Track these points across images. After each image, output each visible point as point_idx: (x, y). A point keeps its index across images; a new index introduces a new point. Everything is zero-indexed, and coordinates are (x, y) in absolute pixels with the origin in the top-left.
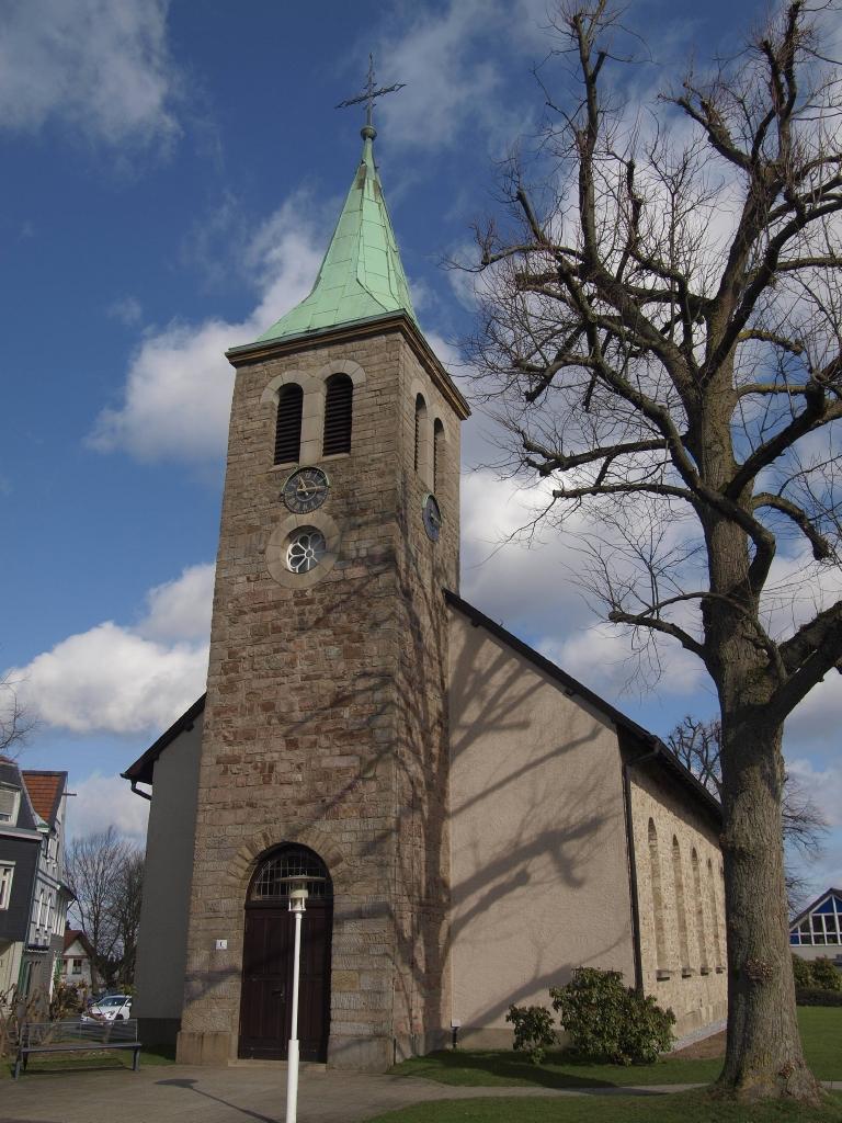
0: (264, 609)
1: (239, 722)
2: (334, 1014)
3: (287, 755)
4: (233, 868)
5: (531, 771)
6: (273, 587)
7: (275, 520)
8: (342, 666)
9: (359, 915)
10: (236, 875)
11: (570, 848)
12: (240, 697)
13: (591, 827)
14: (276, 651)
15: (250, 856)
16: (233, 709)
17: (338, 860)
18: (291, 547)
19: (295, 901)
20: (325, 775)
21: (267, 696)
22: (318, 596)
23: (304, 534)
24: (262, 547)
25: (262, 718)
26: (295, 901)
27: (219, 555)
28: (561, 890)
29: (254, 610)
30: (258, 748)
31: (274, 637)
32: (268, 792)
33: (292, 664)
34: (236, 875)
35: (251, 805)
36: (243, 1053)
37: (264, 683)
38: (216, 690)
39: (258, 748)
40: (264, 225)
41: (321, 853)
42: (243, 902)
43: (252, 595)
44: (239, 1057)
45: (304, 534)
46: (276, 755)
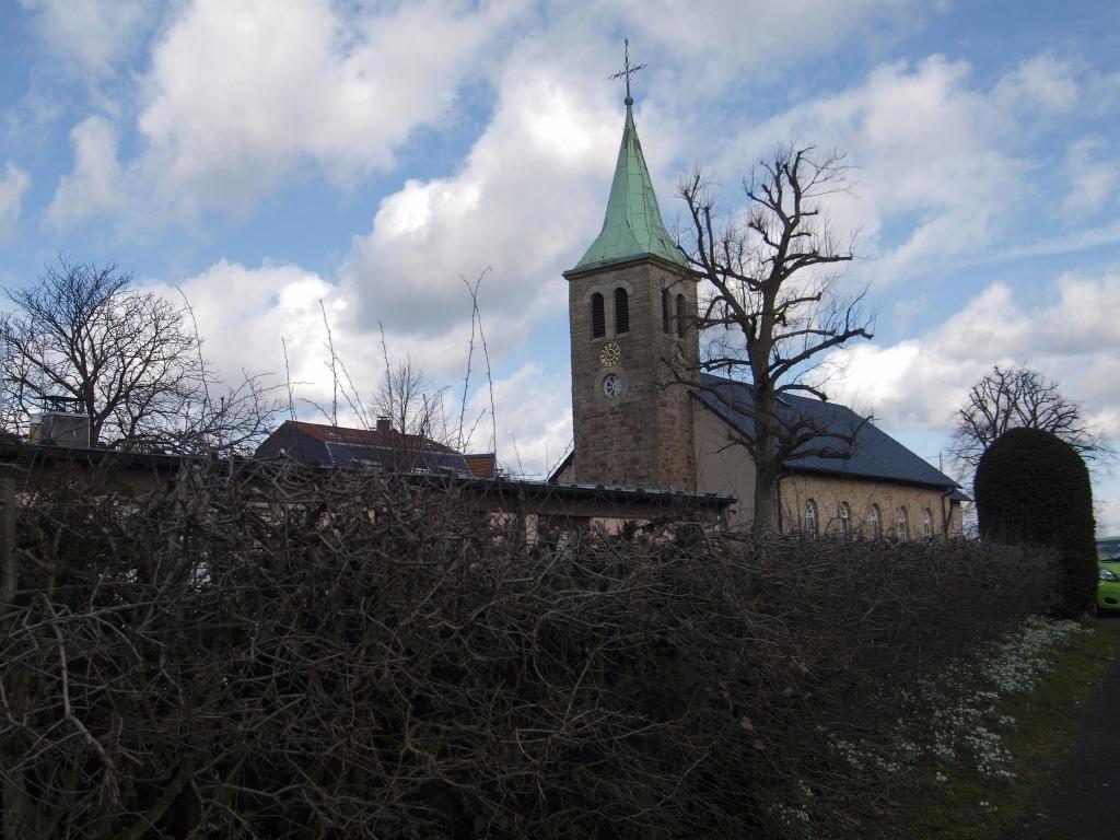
1: (591, 472)
21: (601, 459)
22: (620, 410)
25: (601, 469)
43: (590, 409)
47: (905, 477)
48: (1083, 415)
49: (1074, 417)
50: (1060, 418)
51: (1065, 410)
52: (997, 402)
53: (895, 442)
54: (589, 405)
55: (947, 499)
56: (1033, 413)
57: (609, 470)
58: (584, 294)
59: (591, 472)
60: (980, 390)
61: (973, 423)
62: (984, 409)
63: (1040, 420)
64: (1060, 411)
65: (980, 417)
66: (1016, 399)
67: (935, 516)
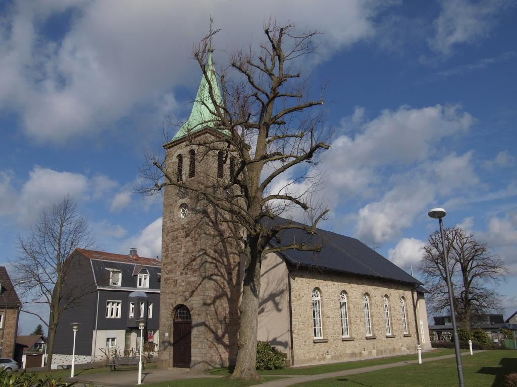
0: (174, 231)
1: (169, 267)
2: (192, 355)
3: (180, 277)
4: (168, 312)
5: (267, 273)
6: (176, 224)
7: (176, 201)
8: (192, 249)
9: (197, 325)
10: (169, 314)
11: (277, 299)
12: (169, 260)
13: (282, 292)
14: (177, 244)
15: (172, 308)
16: (168, 263)
17: (192, 309)
18: (182, 210)
19: (141, 326)
20: (189, 283)
21: (175, 259)
22: (187, 226)
23: (183, 206)
24: (173, 211)
25: (174, 266)
26: (141, 326)
27: (163, 214)
28: (275, 312)
29: (172, 232)
30: (173, 275)
31: (177, 240)
32: (176, 289)
33: (181, 248)
34: (169, 314)
35: (172, 293)
36: (174, 366)
37: (174, 255)
38: (163, 257)
39: (173, 275)
40: (31, 173)
41: (188, 307)
42: (172, 322)
43: (171, 227)
44: (174, 366)
45: (183, 206)
46: (178, 278)
47: (387, 276)
48: (488, 250)
49: (483, 251)
50: (476, 251)
51: (478, 247)
52: (442, 243)
53: (379, 255)
54: (172, 224)
55: (415, 295)
56: (462, 249)
57: (179, 266)
58: (173, 156)
59: (169, 267)
60: (434, 237)
61: (431, 254)
62: (437, 248)
63: (466, 253)
64: (477, 247)
65: (434, 251)
66: (452, 242)
67: (407, 301)
